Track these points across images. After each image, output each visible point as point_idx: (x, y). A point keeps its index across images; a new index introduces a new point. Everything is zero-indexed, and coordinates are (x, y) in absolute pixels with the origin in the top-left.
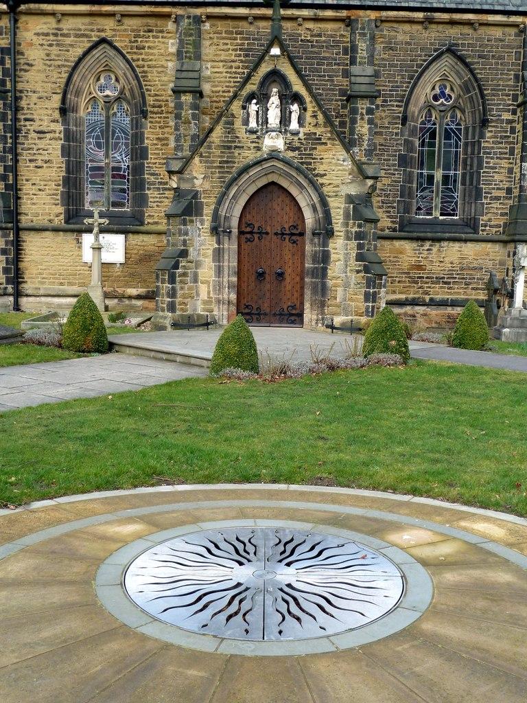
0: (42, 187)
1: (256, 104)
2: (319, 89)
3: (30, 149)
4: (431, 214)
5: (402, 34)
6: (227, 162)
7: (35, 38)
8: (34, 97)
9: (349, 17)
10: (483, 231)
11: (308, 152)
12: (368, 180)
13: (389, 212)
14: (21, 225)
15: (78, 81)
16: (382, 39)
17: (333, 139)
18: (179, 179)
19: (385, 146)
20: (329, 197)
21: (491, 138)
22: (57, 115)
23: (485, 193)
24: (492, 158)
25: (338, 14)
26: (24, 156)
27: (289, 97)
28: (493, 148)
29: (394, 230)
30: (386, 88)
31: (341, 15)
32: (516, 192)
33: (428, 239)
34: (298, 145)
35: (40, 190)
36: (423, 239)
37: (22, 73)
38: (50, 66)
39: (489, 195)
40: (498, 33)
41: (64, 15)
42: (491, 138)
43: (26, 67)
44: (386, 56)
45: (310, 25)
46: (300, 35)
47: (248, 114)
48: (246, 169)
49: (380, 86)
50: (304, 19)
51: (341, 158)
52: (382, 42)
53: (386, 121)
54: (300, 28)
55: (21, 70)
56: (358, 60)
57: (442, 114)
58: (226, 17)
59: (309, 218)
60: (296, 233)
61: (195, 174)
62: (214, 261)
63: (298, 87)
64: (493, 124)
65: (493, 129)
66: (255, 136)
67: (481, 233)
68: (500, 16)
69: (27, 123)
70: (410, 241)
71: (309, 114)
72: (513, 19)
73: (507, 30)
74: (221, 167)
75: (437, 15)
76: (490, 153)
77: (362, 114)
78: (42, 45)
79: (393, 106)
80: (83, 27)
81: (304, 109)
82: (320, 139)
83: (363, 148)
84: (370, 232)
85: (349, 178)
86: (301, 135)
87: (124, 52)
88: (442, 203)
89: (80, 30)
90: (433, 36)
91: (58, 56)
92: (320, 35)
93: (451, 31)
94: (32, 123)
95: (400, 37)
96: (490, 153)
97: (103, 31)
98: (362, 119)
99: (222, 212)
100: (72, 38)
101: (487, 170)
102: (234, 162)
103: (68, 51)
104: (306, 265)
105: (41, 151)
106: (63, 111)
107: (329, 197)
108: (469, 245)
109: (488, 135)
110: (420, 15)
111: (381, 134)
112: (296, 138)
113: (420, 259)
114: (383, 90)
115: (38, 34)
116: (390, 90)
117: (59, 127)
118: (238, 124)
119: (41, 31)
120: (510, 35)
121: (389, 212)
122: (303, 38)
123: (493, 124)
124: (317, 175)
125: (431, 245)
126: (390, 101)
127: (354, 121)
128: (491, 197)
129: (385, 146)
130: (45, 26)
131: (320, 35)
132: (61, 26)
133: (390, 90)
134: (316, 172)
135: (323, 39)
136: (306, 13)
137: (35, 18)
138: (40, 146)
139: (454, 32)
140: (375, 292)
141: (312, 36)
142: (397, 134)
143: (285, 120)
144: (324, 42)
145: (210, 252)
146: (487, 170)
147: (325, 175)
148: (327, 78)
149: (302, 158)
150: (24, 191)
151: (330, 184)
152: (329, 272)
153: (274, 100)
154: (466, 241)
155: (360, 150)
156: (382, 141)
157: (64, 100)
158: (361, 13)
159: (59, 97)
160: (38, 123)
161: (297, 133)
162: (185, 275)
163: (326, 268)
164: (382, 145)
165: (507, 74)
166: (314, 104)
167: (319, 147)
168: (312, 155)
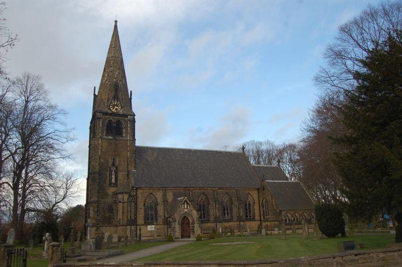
5: (196, 191)
26: (138, 212)
27: (188, 204)
32: (215, 215)
59: (191, 221)
60: (189, 223)
63: (189, 202)
90: (200, 191)
104: (276, 233)
117: (143, 207)
139: (203, 190)
143: (187, 207)
153: (186, 204)
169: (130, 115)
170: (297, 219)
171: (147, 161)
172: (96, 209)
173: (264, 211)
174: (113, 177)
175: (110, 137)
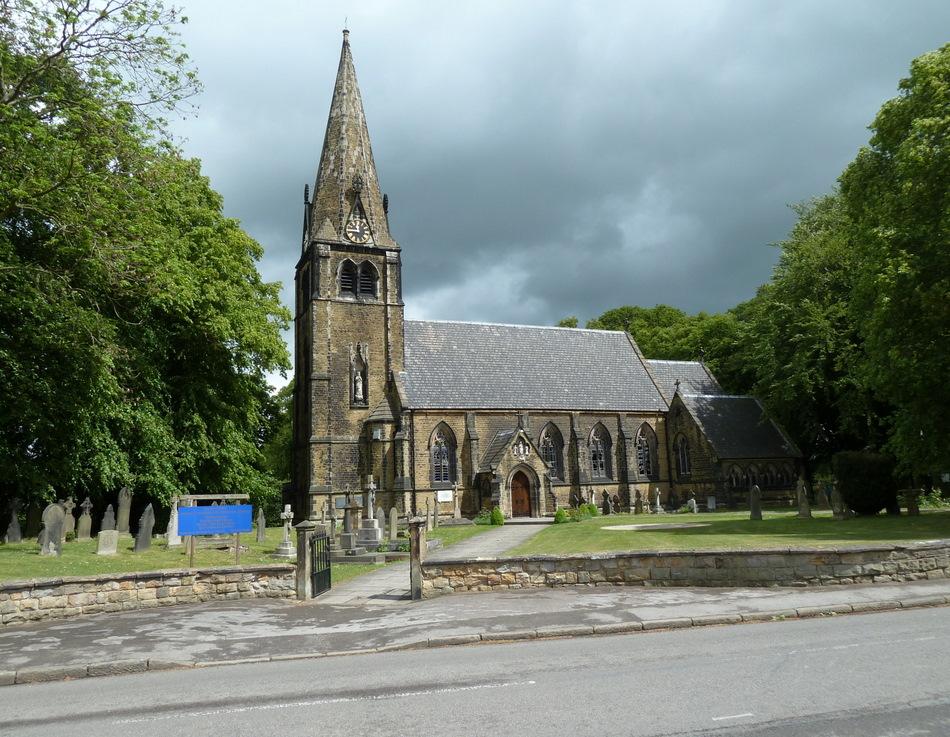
27: (525, 444)
143: (525, 451)
169: (391, 250)
170: (772, 476)
171: (428, 351)
172: (326, 457)
173: (678, 460)
174: (360, 385)
175: (350, 299)
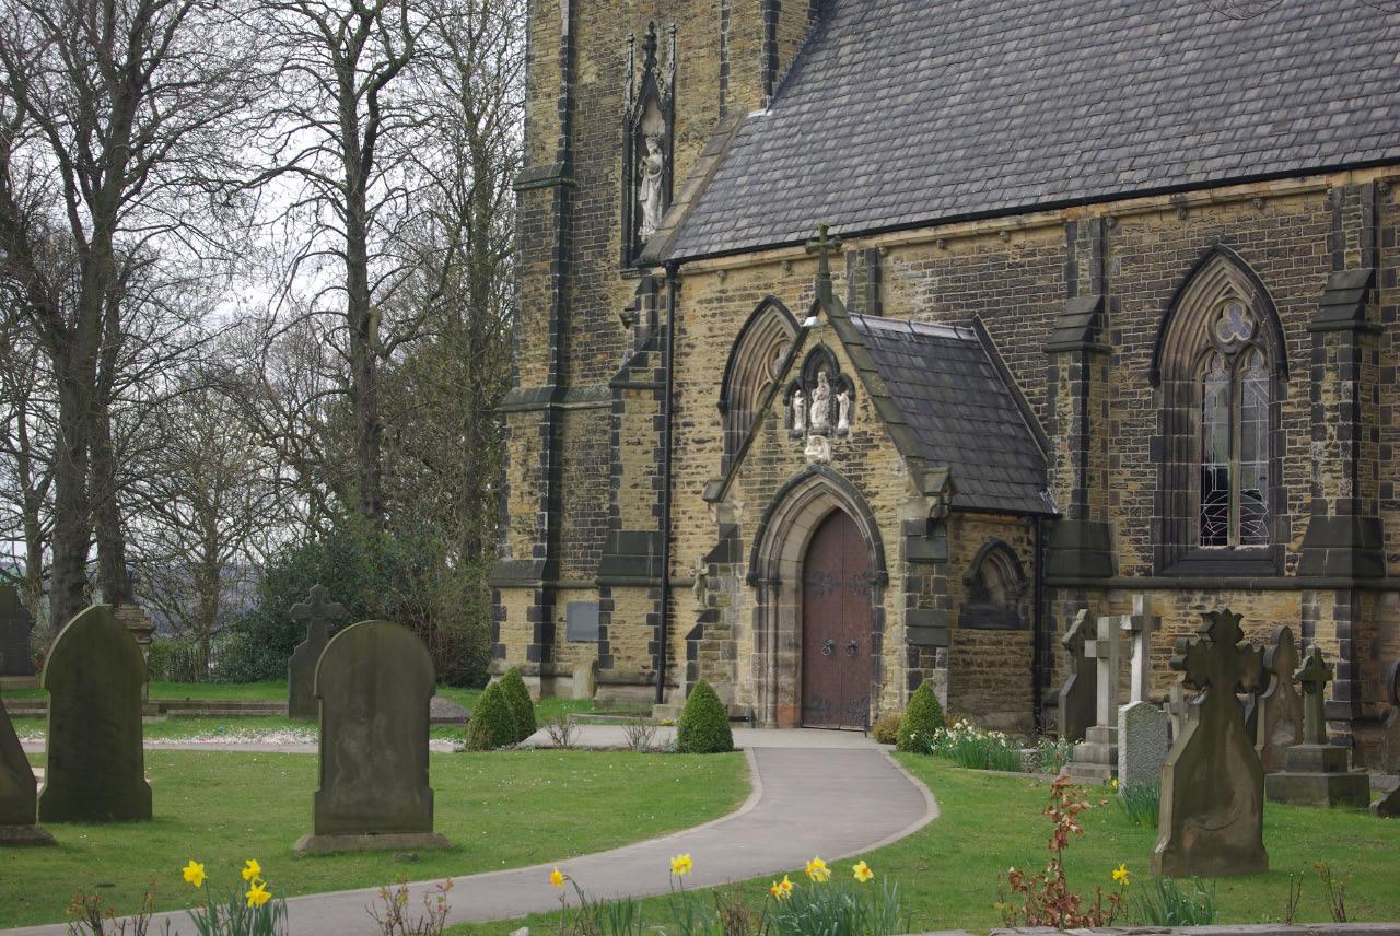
0: (699, 522)
1: (800, 396)
2: (1034, 340)
3: (688, 466)
4: (1224, 542)
6: (768, 482)
7: (697, 307)
8: (694, 390)
9: (1064, 220)
10: (1290, 569)
11: (857, 461)
12: (928, 499)
13: (1138, 541)
14: (672, 580)
15: (745, 362)
16: (1119, 247)
17: (887, 440)
18: (719, 509)
19: (1130, 425)
20: (882, 526)
21: (1295, 396)
22: (718, 416)
23: (1291, 499)
24: (1299, 434)
25: (1050, 218)
28: (1300, 414)
29: (1147, 573)
30: (1128, 327)
31: (1053, 218)
33: (1200, 589)
34: (846, 451)
35: (697, 526)
36: (1191, 589)
37: (684, 359)
38: (712, 345)
39: (1298, 503)
40: (1294, 208)
41: (726, 271)
42: (1295, 396)
43: (687, 350)
44: (1127, 274)
45: (1019, 239)
46: (1007, 257)
47: (793, 411)
48: (786, 491)
49: (1120, 324)
50: (1010, 232)
51: (895, 466)
52: (1120, 252)
53: (1130, 383)
54: (1007, 245)
55: (682, 354)
56: (1079, 287)
57: (1232, 359)
58: (909, 245)
61: (735, 502)
62: (754, 627)
64: (1299, 371)
65: (1299, 380)
66: (798, 443)
67: (1287, 573)
68: (1290, 180)
69: (687, 429)
70: (1168, 592)
71: (859, 404)
72: (1311, 182)
73: (1312, 200)
74: (761, 490)
75: (1191, 195)
76: (1294, 425)
77: (1064, 380)
78: (704, 316)
79: (1139, 356)
80: (748, 285)
81: (852, 398)
82: (871, 440)
83: (1066, 436)
84: (926, 579)
85: (905, 497)
86: (850, 437)
87: (794, 313)
88: (1243, 520)
89: (745, 289)
91: (721, 329)
92: (1033, 254)
93: (1225, 217)
94: (691, 428)
95: (1149, 239)
96: (1294, 425)
97: (768, 286)
98: (1064, 387)
99: (766, 554)
100: (737, 303)
101: (1291, 456)
102: (776, 482)
103: (732, 320)
105: (700, 469)
106: (724, 407)
107: (882, 526)
108: (1266, 597)
109: (1291, 391)
110: (1165, 200)
111: (1122, 405)
112: (844, 441)
113: (1187, 624)
114: (1125, 331)
115: (700, 302)
116: (1135, 330)
118: (781, 424)
119: (703, 297)
120: (1316, 209)
121: (1138, 541)
122: (1010, 261)
123: (1299, 371)
124: (867, 495)
125: (1203, 599)
126: (1136, 348)
127: (1052, 392)
128: (1301, 506)
129: (1130, 425)
130: (708, 290)
131: (1033, 254)
132: (725, 287)
133: (1135, 330)
134: (867, 490)
135: (1038, 258)
136: (1006, 223)
137: (699, 279)
138: (699, 462)
139: (1227, 217)
140: (919, 673)
141: (1023, 256)
142: (1147, 403)
143: (833, 416)
144: (1040, 263)
145: (749, 614)
146: (1291, 456)
147: (877, 493)
148: (1044, 321)
149: (850, 471)
150: (681, 529)
151: (883, 507)
152: (885, 642)
154: (1259, 589)
155: (1063, 439)
156: (1126, 418)
157: (724, 395)
158: (1080, 210)
159: (718, 389)
160: (698, 427)
161: (844, 434)
162: (710, 646)
163: (880, 637)
164: (1125, 425)
165: (1317, 279)
166: (864, 390)
167: (872, 453)
168: (861, 464)
